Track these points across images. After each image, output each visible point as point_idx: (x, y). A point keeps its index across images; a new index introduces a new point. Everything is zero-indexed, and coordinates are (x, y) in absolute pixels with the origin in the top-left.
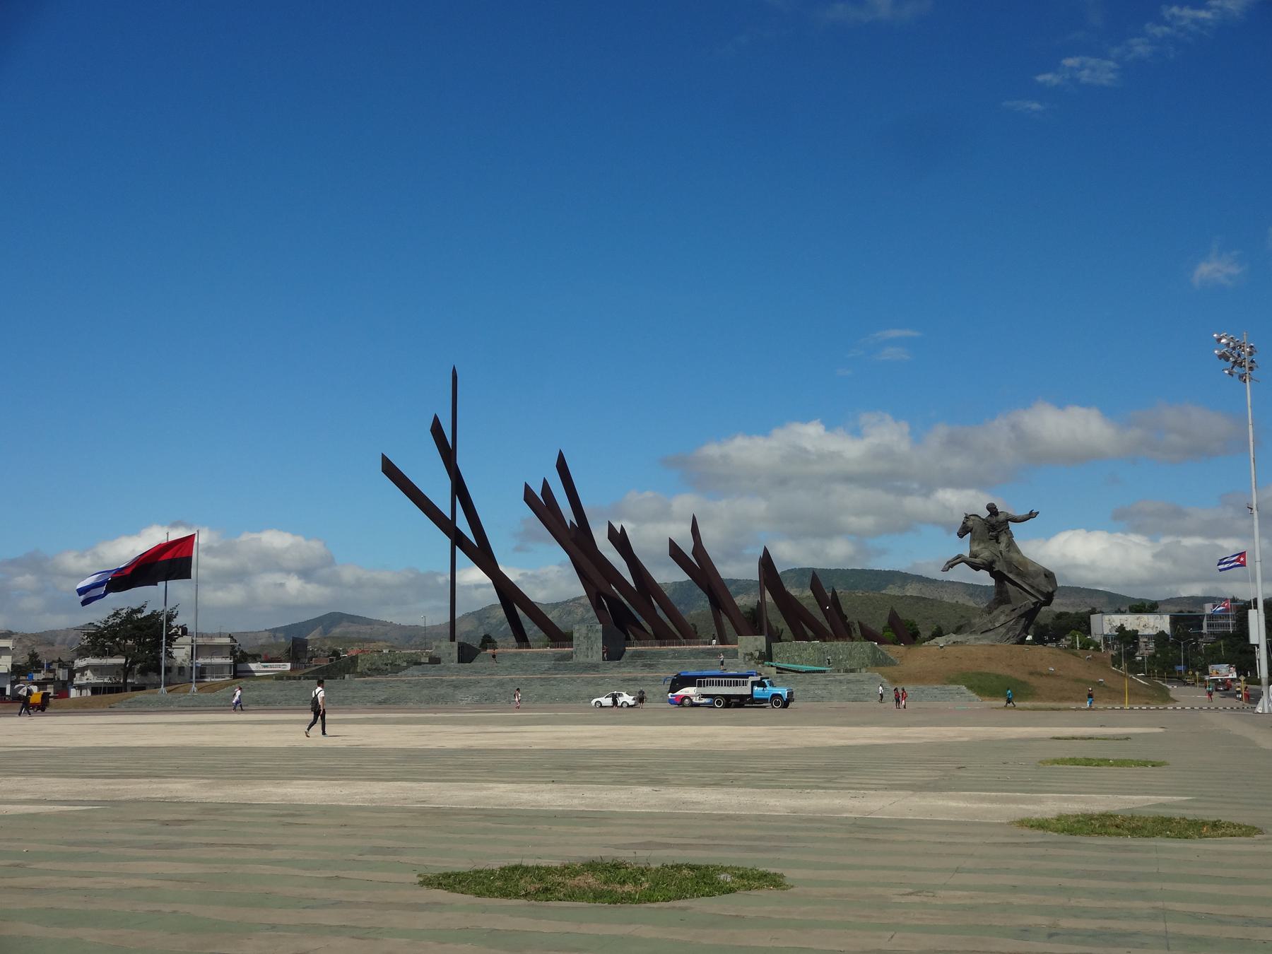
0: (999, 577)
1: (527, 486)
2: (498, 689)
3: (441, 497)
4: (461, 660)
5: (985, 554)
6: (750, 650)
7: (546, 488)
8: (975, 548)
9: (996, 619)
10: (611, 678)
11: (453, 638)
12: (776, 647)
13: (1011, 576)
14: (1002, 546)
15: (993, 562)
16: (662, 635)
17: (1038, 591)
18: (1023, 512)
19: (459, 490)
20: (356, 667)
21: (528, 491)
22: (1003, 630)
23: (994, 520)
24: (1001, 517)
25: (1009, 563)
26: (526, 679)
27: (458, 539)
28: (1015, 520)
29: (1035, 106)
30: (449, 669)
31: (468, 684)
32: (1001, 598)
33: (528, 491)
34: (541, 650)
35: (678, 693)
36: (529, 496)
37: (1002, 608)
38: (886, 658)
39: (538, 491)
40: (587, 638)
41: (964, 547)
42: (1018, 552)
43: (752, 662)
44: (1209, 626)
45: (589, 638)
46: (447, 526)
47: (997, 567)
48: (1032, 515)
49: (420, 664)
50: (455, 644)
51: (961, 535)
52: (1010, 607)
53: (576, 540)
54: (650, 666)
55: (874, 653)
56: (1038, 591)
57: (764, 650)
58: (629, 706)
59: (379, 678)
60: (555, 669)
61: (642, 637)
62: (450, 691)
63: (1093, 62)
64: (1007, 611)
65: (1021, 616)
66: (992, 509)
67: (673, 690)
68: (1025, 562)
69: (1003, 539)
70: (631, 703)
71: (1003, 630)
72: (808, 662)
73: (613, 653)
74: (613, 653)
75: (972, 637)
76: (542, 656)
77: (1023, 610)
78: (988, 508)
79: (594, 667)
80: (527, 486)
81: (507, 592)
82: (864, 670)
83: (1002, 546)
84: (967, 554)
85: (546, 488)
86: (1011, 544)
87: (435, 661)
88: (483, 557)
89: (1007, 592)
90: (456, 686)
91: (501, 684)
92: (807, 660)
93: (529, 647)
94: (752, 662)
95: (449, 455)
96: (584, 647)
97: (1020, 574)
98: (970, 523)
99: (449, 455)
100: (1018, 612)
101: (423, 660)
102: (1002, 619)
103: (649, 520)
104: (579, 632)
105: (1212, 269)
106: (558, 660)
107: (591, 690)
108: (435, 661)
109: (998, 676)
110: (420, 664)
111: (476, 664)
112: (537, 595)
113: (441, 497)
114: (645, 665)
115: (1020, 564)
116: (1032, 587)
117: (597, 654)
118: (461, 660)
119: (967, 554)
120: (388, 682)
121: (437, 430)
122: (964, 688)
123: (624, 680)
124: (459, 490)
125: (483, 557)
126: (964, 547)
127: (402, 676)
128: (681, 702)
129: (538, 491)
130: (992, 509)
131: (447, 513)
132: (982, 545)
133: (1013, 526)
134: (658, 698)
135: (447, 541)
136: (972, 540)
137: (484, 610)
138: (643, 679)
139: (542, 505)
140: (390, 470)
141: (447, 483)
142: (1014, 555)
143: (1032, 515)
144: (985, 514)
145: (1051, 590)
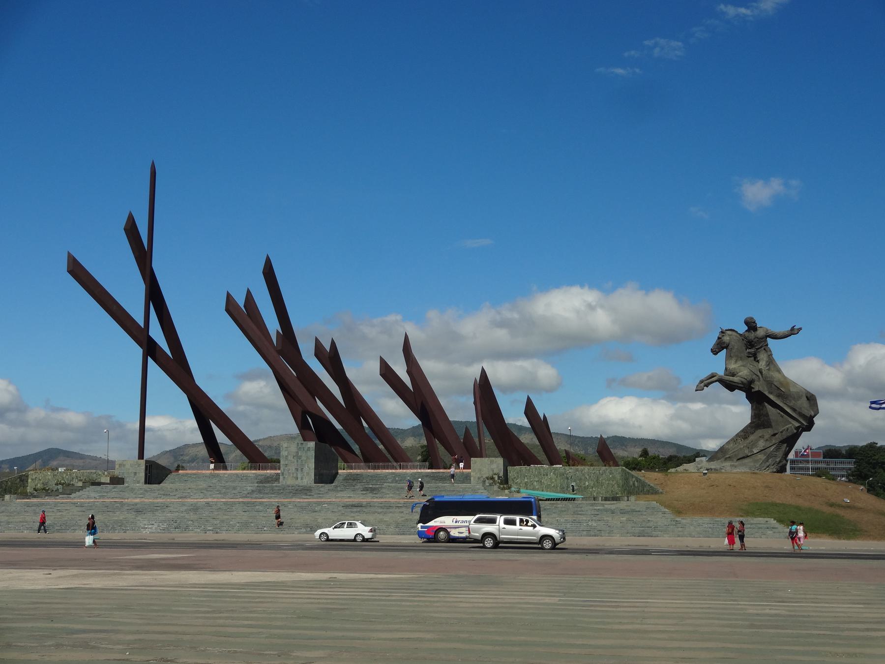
0: (756, 398)
1: (229, 296)
2: (192, 516)
3: (134, 302)
4: (149, 480)
5: (744, 371)
6: (487, 473)
7: (249, 298)
8: (733, 366)
9: (754, 444)
10: (329, 503)
11: (141, 455)
12: (513, 471)
13: (771, 397)
14: (762, 364)
15: (752, 382)
16: (371, 458)
17: (801, 414)
19: (154, 296)
20: (25, 487)
21: (229, 298)
22: (762, 457)
23: (752, 335)
24: (760, 333)
25: (770, 383)
26: (225, 503)
27: (150, 349)
28: (775, 337)
29: (620, 71)
30: (132, 490)
31: (154, 509)
32: (759, 421)
33: (229, 298)
34: (238, 472)
35: (432, 523)
36: (231, 307)
37: (760, 432)
38: (643, 485)
39: (241, 302)
40: (297, 456)
41: (718, 364)
42: (779, 371)
43: (496, 488)
44: (792, 469)
45: (299, 460)
47: (757, 387)
48: (793, 331)
49: (99, 484)
50: (143, 462)
51: (715, 352)
52: (770, 431)
53: (280, 351)
54: (372, 490)
55: (627, 479)
56: (801, 414)
57: (501, 474)
58: (365, 540)
59: (48, 500)
60: (260, 492)
61: (349, 456)
62: (131, 516)
63: (662, 41)
64: (767, 436)
65: (782, 442)
66: (751, 325)
67: (424, 519)
68: (786, 382)
69: (762, 356)
70: (368, 535)
71: (762, 457)
72: (548, 488)
73: (325, 475)
74: (325, 475)
75: (727, 464)
76: (242, 478)
77: (785, 435)
78: (747, 323)
79: (305, 491)
80: (229, 296)
81: (205, 411)
83: (762, 364)
84: (721, 372)
85: (249, 298)
86: (771, 362)
87: (117, 481)
88: (178, 368)
89: (767, 415)
90: (139, 511)
91: (195, 509)
92: (556, 487)
93: (225, 468)
94: (496, 488)
95: (143, 257)
96: (292, 468)
97: (782, 395)
98: (726, 339)
99: (143, 257)
100: (779, 437)
101: (103, 480)
102: (761, 444)
103: (366, 335)
104: (288, 451)
105: (758, 193)
106: (261, 482)
107: (307, 518)
108: (117, 481)
109: (798, 508)
110: (99, 484)
111: (166, 485)
113: (134, 302)
114: (366, 489)
115: (781, 383)
116: (794, 410)
117: (308, 477)
118: (149, 480)
119: (721, 372)
120: (56, 505)
122: (773, 522)
123: (346, 506)
124: (154, 296)
125: (178, 368)
126: (718, 364)
127: (77, 498)
128: (433, 537)
129: (241, 302)
130: (751, 325)
131: (141, 322)
132: (740, 363)
134: (392, 529)
135: (138, 351)
136: (729, 357)
137: (179, 448)
138: (369, 505)
139: (245, 316)
140: (77, 271)
141: (140, 288)
142: (776, 375)
143: (793, 331)
144: (742, 329)
145: (813, 414)
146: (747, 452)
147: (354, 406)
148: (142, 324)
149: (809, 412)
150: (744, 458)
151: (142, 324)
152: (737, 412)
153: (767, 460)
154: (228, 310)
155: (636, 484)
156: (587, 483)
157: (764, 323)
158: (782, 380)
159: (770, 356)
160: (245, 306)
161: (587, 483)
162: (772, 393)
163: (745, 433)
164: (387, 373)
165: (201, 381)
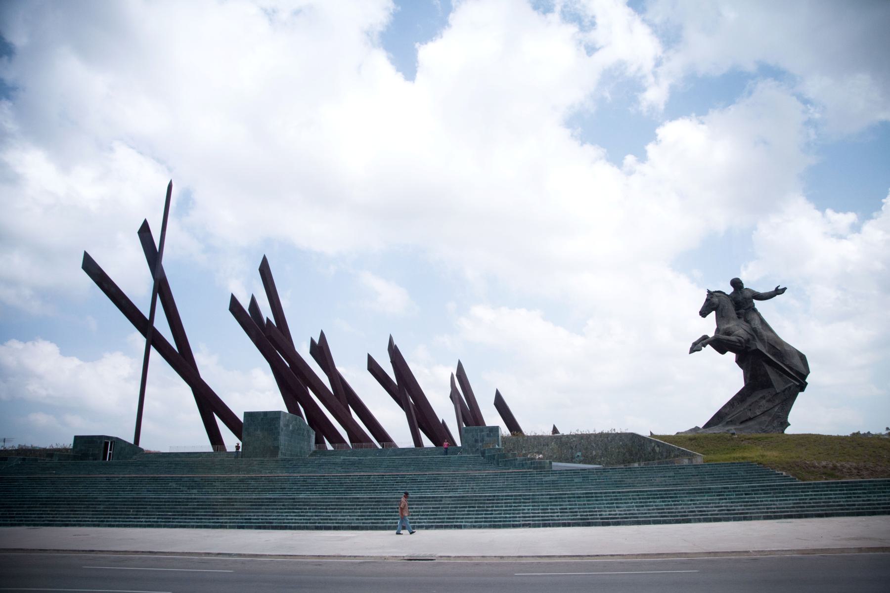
3: (138, 285)
5: (739, 330)
7: (253, 304)
19: (162, 288)
27: (154, 340)
37: (760, 394)
46: (144, 325)
48: (779, 291)
51: (704, 313)
66: (736, 284)
82: (731, 356)
85: (253, 304)
88: (182, 361)
98: (715, 300)
112: (239, 408)
115: (776, 342)
121: (144, 231)
124: (162, 288)
125: (182, 361)
126: (709, 326)
129: (245, 304)
130: (736, 284)
133: (758, 304)
135: (140, 341)
139: (246, 318)
143: (779, 291)
144: (729, 290)
146: (749, 414)
147: (344, 397)
148: (147, 316)
149: (804, 372)
150: (747, 420)
151: (147, 316)
152: (726, 376)
154: (231, 309)
155: (657, 449)
156: (594, 453)
157: (749, 283)
159: (759, 315)
160: (249, 310)
161: (594, 453)
163: (740, 398)
164: (374, 368)
165: (204, 375)
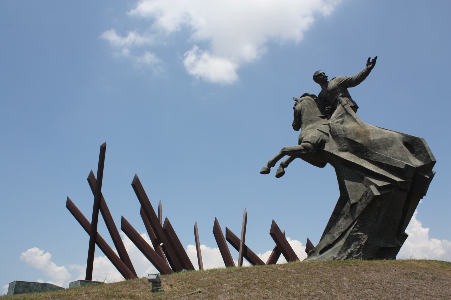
18: (363, 67)
19: (100, 205)
22: (341, 243)
66: (320, 78)
115: (357, 135)
124: (100, 205)
130: (320, 78)
143: (372, 63)
145: (416, 163)
153: (347, 245)
158: (358, 129)
162: (346, 151)
